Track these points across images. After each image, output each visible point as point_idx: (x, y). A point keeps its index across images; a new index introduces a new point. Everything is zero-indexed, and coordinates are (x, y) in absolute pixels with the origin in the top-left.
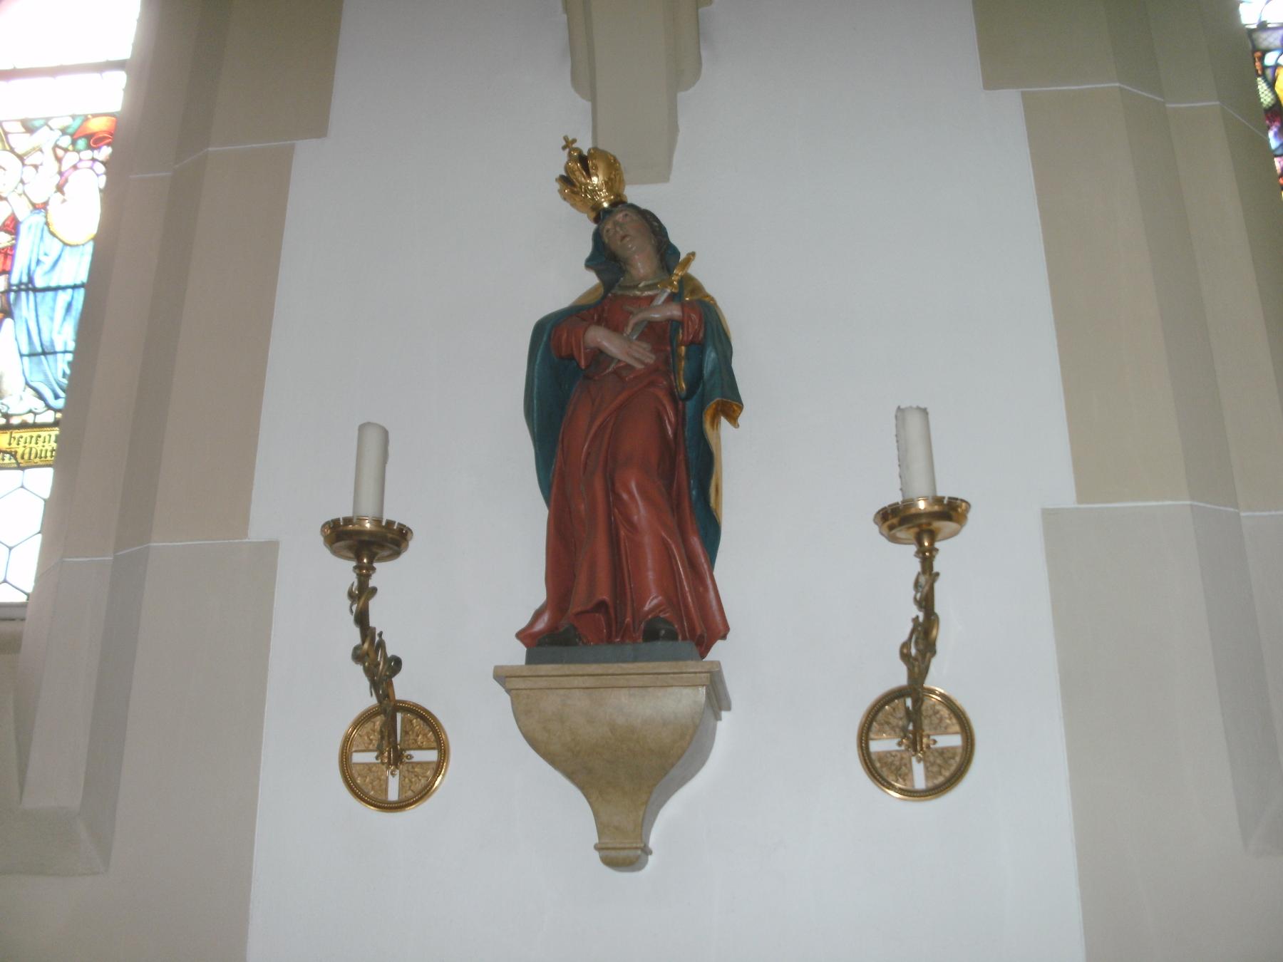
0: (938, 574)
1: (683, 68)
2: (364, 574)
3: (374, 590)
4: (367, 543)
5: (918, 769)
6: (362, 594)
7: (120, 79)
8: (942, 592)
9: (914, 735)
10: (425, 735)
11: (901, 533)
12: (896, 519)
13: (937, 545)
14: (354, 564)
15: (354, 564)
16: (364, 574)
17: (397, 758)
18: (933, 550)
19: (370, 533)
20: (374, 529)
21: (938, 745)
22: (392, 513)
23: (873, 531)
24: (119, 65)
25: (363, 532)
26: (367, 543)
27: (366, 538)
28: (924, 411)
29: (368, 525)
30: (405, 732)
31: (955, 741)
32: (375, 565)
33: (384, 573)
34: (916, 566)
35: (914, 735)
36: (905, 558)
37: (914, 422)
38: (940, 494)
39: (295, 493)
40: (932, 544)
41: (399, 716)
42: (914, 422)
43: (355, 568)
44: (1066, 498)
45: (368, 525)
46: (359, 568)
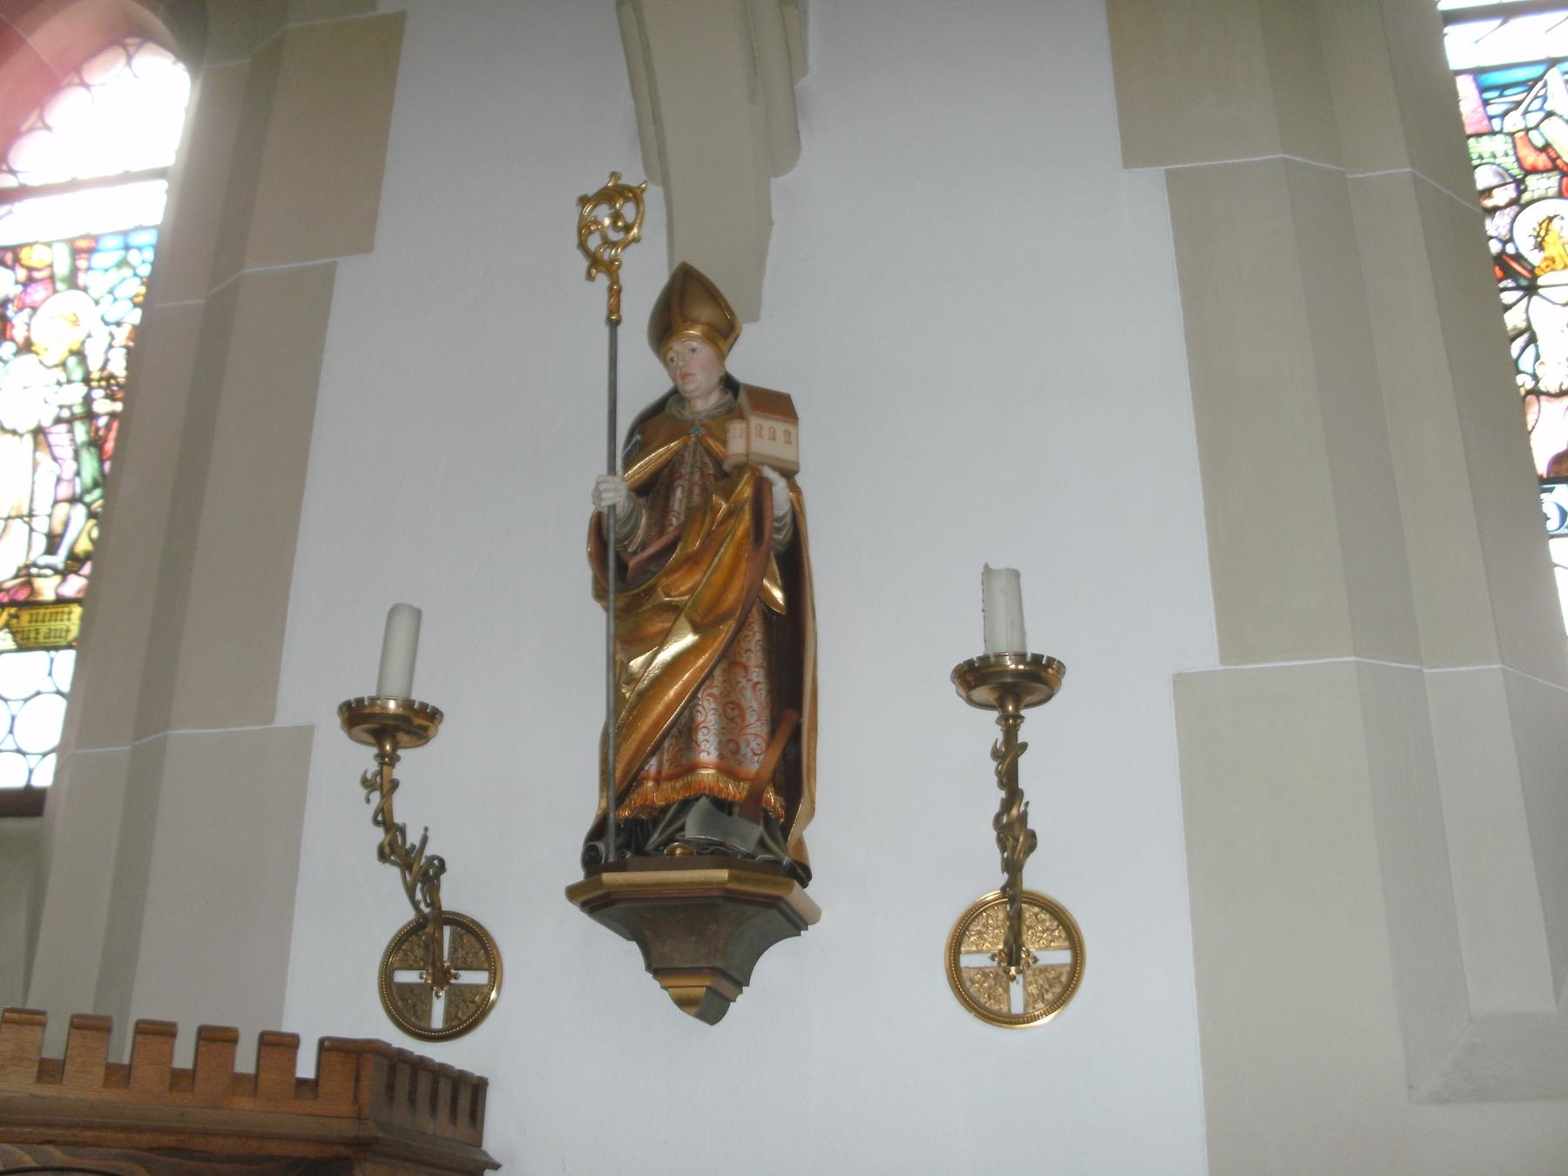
0: (1024, 746)
1: (780, 145)
2: (1011, 726)
3: (1024, 746)
4: (390, 726)
5: (468, 978)
6: (1008, 756)
7: (162, 185)
8: (1028, 771)
9: (1016, 950)
10: (476, 954)
11: (982, 693)
12: (975, 676)
13: (400, 752)
14: (375, 750)
15: (375, 750)
16: (1011, 726)
17: (442, 977)
18: (1018, 718)
19: (395, 716)
20: (400, 711)
21: (1041, 963)
22: (422, 694)
23: (951, 689)
24: (161, 174)
25: (386, 715)
26: (1009, 684)
27: (391, 722)
28: (418, 614)
29: (392, 705)
30: (454, 950)
31: (1065, 957)
32: (1023, 712)
33: (411, 763)
34: (997, 734)
35: (1016, 950)
36: (986, 727)
37: (403, 623)
38: (413, 697)
39: (323, 666)
40: (1017, 709)
41: (447, 930)
42: (403, 623)
43: (377, 756)
44: (1204, 654)
45: (392, 705)
46: (1004, 718)
